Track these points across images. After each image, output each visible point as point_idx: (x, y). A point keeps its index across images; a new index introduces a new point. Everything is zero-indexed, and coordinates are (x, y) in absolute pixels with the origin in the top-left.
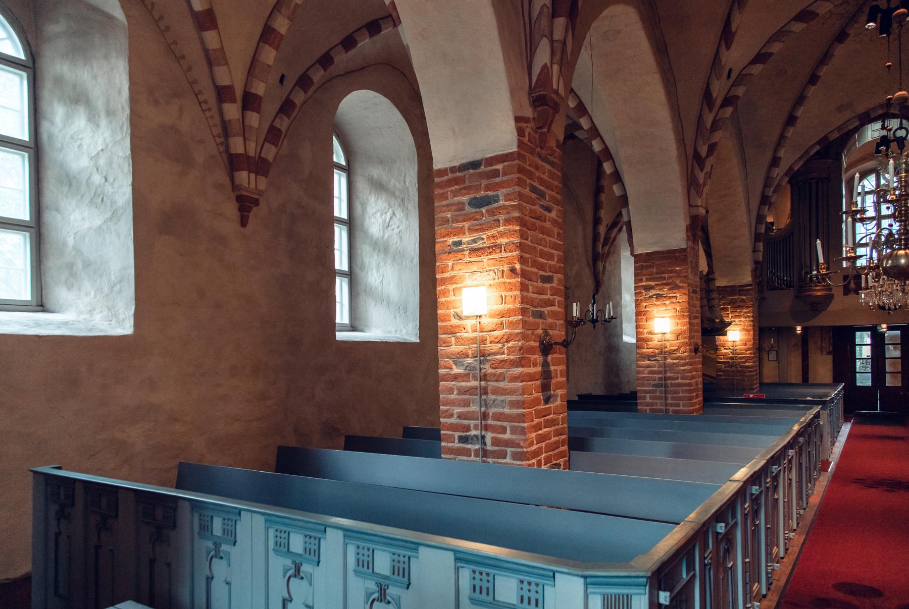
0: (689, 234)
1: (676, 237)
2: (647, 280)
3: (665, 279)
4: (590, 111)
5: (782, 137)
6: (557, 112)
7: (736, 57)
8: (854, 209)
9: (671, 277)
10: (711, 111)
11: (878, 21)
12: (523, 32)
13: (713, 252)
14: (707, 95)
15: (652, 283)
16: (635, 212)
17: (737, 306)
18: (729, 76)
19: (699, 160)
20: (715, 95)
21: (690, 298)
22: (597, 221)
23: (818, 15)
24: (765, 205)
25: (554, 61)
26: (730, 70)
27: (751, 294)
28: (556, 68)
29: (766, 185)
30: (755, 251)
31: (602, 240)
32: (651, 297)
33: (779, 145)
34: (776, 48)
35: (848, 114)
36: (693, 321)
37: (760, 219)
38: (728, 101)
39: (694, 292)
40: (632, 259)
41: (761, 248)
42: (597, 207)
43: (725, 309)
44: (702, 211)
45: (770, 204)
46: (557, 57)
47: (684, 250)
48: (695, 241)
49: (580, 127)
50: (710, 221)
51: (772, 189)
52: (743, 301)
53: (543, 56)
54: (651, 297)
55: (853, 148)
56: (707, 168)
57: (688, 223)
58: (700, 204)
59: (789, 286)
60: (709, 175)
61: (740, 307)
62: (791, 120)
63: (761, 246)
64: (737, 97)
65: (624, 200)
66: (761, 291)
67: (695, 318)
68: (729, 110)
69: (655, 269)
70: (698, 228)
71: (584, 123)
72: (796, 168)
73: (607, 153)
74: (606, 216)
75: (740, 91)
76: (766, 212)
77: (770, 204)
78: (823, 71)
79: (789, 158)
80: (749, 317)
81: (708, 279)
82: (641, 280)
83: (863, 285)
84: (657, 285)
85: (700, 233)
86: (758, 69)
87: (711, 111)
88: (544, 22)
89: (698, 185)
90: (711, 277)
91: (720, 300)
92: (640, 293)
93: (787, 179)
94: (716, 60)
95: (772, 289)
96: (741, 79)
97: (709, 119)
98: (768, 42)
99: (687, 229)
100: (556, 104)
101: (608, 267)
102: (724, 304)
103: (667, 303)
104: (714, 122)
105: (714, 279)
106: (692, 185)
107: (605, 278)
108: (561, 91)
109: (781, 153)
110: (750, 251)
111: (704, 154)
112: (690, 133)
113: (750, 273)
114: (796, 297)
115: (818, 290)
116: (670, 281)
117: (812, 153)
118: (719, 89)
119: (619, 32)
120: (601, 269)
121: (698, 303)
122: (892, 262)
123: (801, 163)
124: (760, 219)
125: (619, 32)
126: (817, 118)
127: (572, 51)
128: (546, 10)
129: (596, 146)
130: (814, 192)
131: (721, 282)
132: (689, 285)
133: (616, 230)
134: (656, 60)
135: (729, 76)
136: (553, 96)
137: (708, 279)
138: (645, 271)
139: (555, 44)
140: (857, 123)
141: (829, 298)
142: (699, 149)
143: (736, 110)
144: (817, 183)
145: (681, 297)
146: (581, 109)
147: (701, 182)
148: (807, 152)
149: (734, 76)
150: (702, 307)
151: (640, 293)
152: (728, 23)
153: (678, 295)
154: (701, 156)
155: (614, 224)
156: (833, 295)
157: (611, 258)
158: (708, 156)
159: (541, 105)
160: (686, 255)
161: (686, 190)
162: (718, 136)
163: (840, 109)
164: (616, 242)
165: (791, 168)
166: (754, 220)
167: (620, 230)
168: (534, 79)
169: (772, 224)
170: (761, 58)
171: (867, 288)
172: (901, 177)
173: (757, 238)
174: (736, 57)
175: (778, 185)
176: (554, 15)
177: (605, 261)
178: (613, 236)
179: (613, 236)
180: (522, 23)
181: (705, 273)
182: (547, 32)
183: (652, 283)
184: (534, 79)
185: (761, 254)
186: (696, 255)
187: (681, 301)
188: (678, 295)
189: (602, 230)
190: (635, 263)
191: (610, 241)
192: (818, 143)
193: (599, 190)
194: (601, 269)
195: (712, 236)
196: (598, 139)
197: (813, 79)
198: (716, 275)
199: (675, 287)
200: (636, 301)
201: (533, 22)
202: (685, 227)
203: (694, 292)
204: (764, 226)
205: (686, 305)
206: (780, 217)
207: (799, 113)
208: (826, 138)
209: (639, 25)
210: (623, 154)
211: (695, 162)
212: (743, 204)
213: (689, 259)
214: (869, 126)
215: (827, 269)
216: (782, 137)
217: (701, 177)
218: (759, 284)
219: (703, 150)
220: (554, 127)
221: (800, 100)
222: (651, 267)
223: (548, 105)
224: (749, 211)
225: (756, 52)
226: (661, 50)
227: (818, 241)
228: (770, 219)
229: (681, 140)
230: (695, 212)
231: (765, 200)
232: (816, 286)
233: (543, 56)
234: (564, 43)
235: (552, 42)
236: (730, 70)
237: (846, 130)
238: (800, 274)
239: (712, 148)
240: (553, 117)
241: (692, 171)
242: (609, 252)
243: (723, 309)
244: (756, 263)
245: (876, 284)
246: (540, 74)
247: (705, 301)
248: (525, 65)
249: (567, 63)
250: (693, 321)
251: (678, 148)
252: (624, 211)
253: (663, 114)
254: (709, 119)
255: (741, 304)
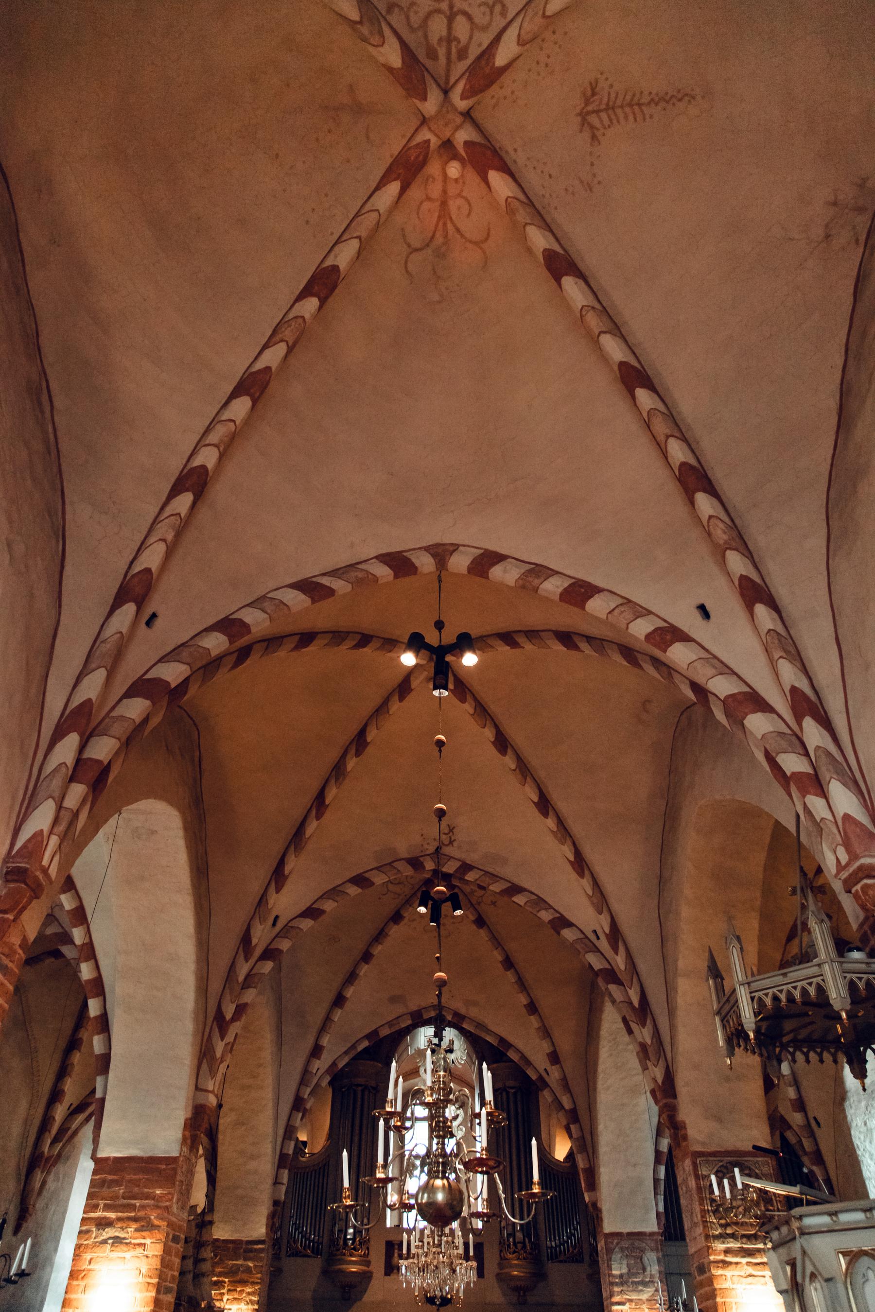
0: (187, 1133)
1: (165, 1138)
2: (107, 1208)
3: (132, 1208)
4: (89, 919)
5: (328, 1019)
6: (37, 897)
7: (287, 902)
8: (388, 1109)
9: (143, 1207)
10: (247, 960)
11: (430, 906)
12: (24, 782)
13: (219, 1175)
14: (246, 940)
15: (112, 1215)
16: (115, 1090)
17: (238, 1279)
18: (274, 924)
19: (221, 1023)
20: (254, 941)
21: (167, 1251)
22: (56, 1096)
23: (373, 884)
24: (298, 1111)
25: (55, 830)
26: (277, 917)
27: (261, 1259)
28: (54, 840)
29: (303, 1081)
30: (276, 1182)
31: (54, 1131)
32: (104, 1242)
33: (323, 1029)
34: (328, 906)
35: (399, 1009)
36: (161, 1297)
37: (289, 1132)
38: (269, 954)
39: (175, 1239)
40: (91, 1165)
41: (285, 1180)
42: (63, 1072)
43: (219, 1284)
44: (212, 1100)
45: (305, 1112)
46: (61, 828)
47: (174, 1160)
48: (193, 1148)
49: (70, 941)
50: (225, 1122)
51: (309, 1090)
52: (248, 1270)
53: (42, 818)
54: (104, 1242)
55: (404, 1056)
56: (229, 1038)
57: (189, 1115)
58: (211, 1088)
59: (317, 1252)
60: (230, 1048)
61: (243, 1282)
62: (339, 1001)
63: (285, 1175)
64: (280, 951)
65: (104, 1063)
66: (276, 1257)
67: (168, 1290)
68: (268, 966)
69: (125, 1186)
70: (203, 1127)
71: (78, 935)
72: (341, 1065)
73: (98, 986)
74: (72, 1090)
75: (285, 945)
76: (298, 1123)
77: (305, 1112)
78: (377, 950)
79: (334, 1051)
80: (252, 1302)
81: (203, 1221)
82: (95, 1207)
83: (405, 1251)
84: (119, 1219)
85: (204, 1138)
86: (307, 924)
87: (247, 960)
88: (56, 784)
89: (213, 1057)
90: (208, 1218)
91: (214, 1265)
92: (88, 1232)
93: (328, 1078)
94: (262, 900)
95: (292, 1255)
96: (287, 931)
97: (243, 970)
98: (321, 897)
99: (185, 1124)
100: (39, 885)
101: (51, 1185)
102: (219, 1275)
103: (128, 1255)
104: (248, 976)
105: (211, 1223)
106: (205, 1056)
107: (40, 1205)
108: (53, 871)
109: (325, 1041)
110: (269, 1181)
111: (228, 1016)
112: (216, 985)
113: (264, 1221)
114: (325, 1272)
115: (354, 1263)
116: (141, 1214)
117: (360, 1048)
118: (261, 935)
119: (153, 832)
120: (37, 1185)
121: (177, 1261)
122: (429, 1197)
123: (346, 1060)
124: (289, 1132)
125: (153, 832)
126: (366, 1009)
127: (83, 830)
128: (64, 769)
129: (86, 972)
130: (359, 1103)
131: (221, 1232)
132: (170, 1225)
133: (81, 1117)
134: (192, 881)
135: (274, 924)
136: (38, 873)
137: (203, 1221)
138: (105, 1191)
139: (63, 812)
140: (409, 1022)
141: (366, 1277)
142: (223, 1008)
143: (278, 969)
144: (363, 1091)
145: (153, 1245)
146: (80, 916)
147: (218, 1055)
148: (353, 1047)
149: (280, 924)
150: (182, 1273)
151: (88, 1232)
152: (281, 863)
153: (148, 1241)
154: (224, 1018)
155: (80, 1108)
156: (371, 1273)
157: (61, 1168)
158: (234, 1019)
159: (16, 881)
160: (175, 1170)
161: (196, 1061)
162: (249, 996)
163: (393, 1000)
164: (76, 1140)
165: (334, 1064)
166: (281, 1132)
167: (87, 1120)
168: (19, 844)
169: (305, 1143)
170: (311, 912)
171: (409, 1256)
172: (439, 1077)
173: (282, 1161)
174: (287, 902)
175: (317, 1085)
176: (72, 779)
177: (49, 1173)
178: (74, 1127)
179: (74, 1127)
180: (27, 774)
181: (199, 1210)
182: (57, 794)
183: (112, 1215)
184: (19, 844)
185: (284, 1188)
186: (191, 1173)
187: (150, 1254)
188: (148, 1241)
189: (60, 1112)
190: (95, 1172)
191: (66, 1136)
192: (367, 1037)
193: (73, 1044)
194: (37, 1185)
195: (221, 1149)
196: (91, 963)
197: (367, 957)
198: (217, 1216)
199: (147, 1226)
200: (78, 1247)
201: (42, 777)
202: (183, 1122)
203: (175, 1239)
204: (292, 1144)
205: (156, 1263)
206: (314, 1136)
207: (349, 993)
208: (375, 1032)
209: (181, 833)
210: (118, 989)
211: (215, 1023)
212: (270, 1105)
213: (179, 1177)
214: (422, 1029)
215: (356, 1199)
216: (328, 1019)
217: (219, 1047)
218: (276, 1243)
219: (229, 1011)
220: (25, 916)
221: (351, 978)
222: (117, 1183)
223: (26, 884)
224: (276, 1118)
225: (308, 905)
226: (201, 870)
227: (345, 1154)
228: (303, 1137)
229: (203, 989)
230: (202, 1099)
231: (298, 1104)
232: (351, 1255)
233: (42, 818)
234: (76, 815)
235: (60, 808)
236: (277, 917)
237: (397, 1028)
238: (332, 1232)
239: (241, 1010)
240: (29, 902)
241: (209, 1035)
242: (59, 1155)
243: (216, 1283)
244: (276, 1203)
245: (420, 1251)
246: (29, 840)
247: (190, 1263)
248: (12, 823)
249: (74, 842)
250: (161, 1297)
251: (197, 1001)
252: (99, 1080)
253: (186, 949)
254: (243, 970)
255: (245, 1276)
